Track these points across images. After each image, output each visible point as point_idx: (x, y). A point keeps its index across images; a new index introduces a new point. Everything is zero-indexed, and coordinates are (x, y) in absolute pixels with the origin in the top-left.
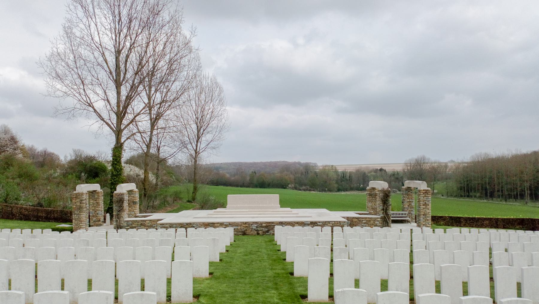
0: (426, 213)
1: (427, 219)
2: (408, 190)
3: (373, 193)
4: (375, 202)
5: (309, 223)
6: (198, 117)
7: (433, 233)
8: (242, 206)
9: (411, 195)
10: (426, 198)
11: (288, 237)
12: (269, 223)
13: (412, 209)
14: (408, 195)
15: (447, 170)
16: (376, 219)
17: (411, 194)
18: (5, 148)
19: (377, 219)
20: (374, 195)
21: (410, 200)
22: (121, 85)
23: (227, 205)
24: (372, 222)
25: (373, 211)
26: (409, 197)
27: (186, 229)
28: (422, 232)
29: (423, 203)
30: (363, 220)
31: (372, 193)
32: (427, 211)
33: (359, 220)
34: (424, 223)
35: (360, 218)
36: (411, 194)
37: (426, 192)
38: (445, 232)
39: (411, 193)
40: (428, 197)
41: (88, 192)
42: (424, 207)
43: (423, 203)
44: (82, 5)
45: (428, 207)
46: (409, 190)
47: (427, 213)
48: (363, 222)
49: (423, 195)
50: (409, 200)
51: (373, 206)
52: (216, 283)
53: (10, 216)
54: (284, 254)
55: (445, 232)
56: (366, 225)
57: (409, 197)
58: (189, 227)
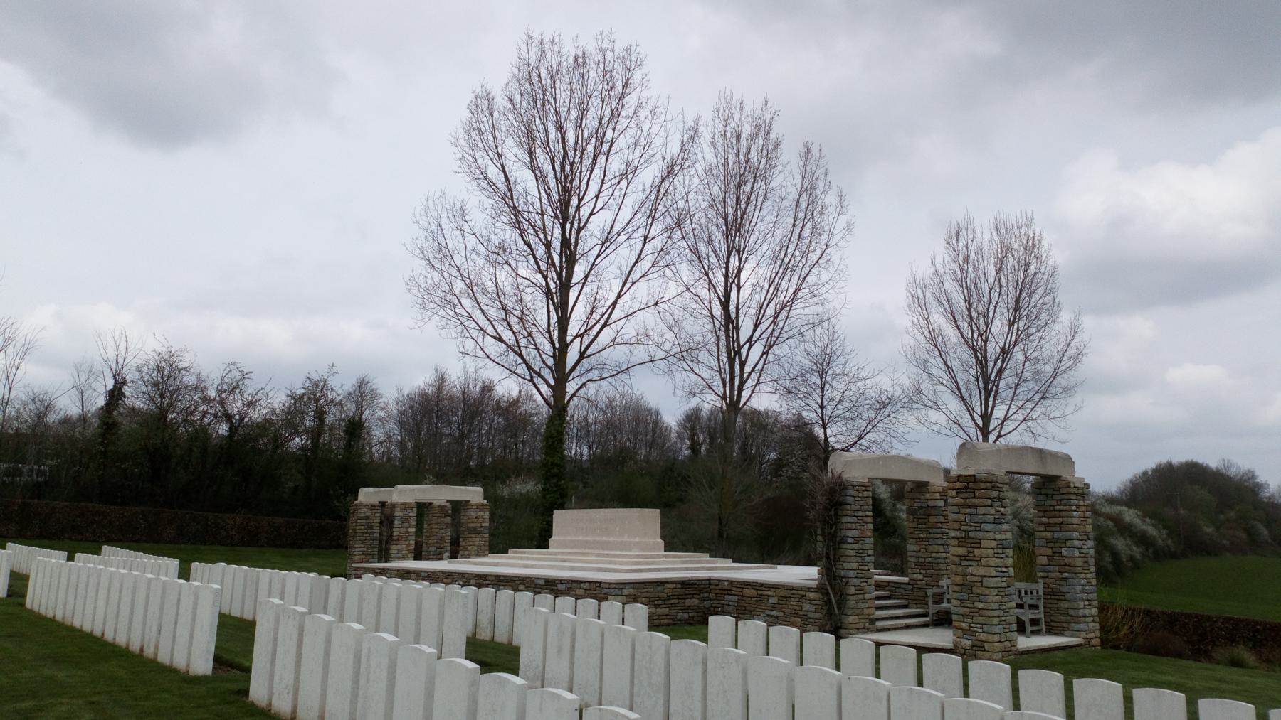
2: (1043, 491)
3: (919, 505)
6: (975, 343)
9: (1060, 511)
10: (968, 510)
14: (1048, 514)
15: (525, 456)
16: (804, 593)
18: (789, 457)
20: (922, 511)
21: (1056, 535)
24: (793, 603)
25: (920, 577)
26: (1052, 521)
27: (576, 599)
29: (958, 534)
30: (770, 593)
31: (916, 504)
32: (975, 571)
33: (760, 592)
34: (964, 625)
37: (966, 488)
39: (1059, 502)
40: (976, 507)
42: (961, 551)
43: (958, 534)
45: (977, 552)
46: (1050, 492)
47: (975, 579)
49: (957, 500)
50: (1048, 534)
51: (920, 554)
52: (37, 409)
57: (1052, 521)
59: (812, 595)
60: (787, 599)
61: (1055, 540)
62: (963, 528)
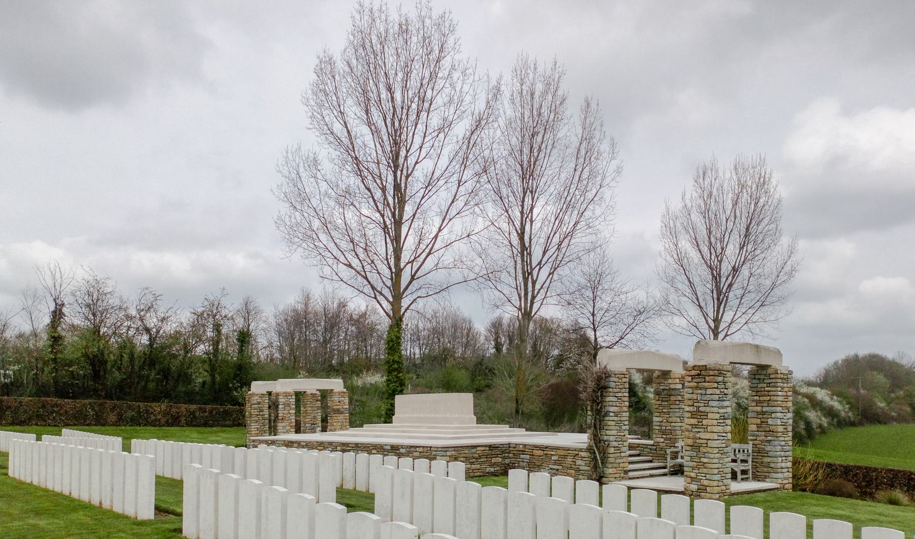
0: (698, 441)
1: (702, 460)
2: (757, 377)
4: (669, 413)
5: (389, 448)
7: (124, 449)
8: (422, 415)
10: (699, 391)
11: (563, 501)
12: (411, 447)
13: (769, 438)
16: (577, 452)
17: (767, 389)
19: (580, 453)
21: (765, 409)
22: (402, 298)
23: (394, 415)
24: (569, 460)
25: (662, 440)
26: (761, 398)
28: (692, 517)
29: (691, 409)
30: (552, 453)
32: (702, 435)
34: (693, 475)
35: (547, 447)
36: (767, 389)
37: (699, 375)
38: (127, 448)
41: (267, 392)
42: (694, 421)
43: (691, 409)
44: (543, 262)
45: (705, 422)
48: (553, 458)
50: (759, 409)
53: (230, 420)
54: (159, 492)
55: (127, 448)
56: (558, 467)
57: (761, 398)
58: (511, 469)
59: (583, 454)
60: (565, 456)
61: (763, 413)
62: (695, 404)
